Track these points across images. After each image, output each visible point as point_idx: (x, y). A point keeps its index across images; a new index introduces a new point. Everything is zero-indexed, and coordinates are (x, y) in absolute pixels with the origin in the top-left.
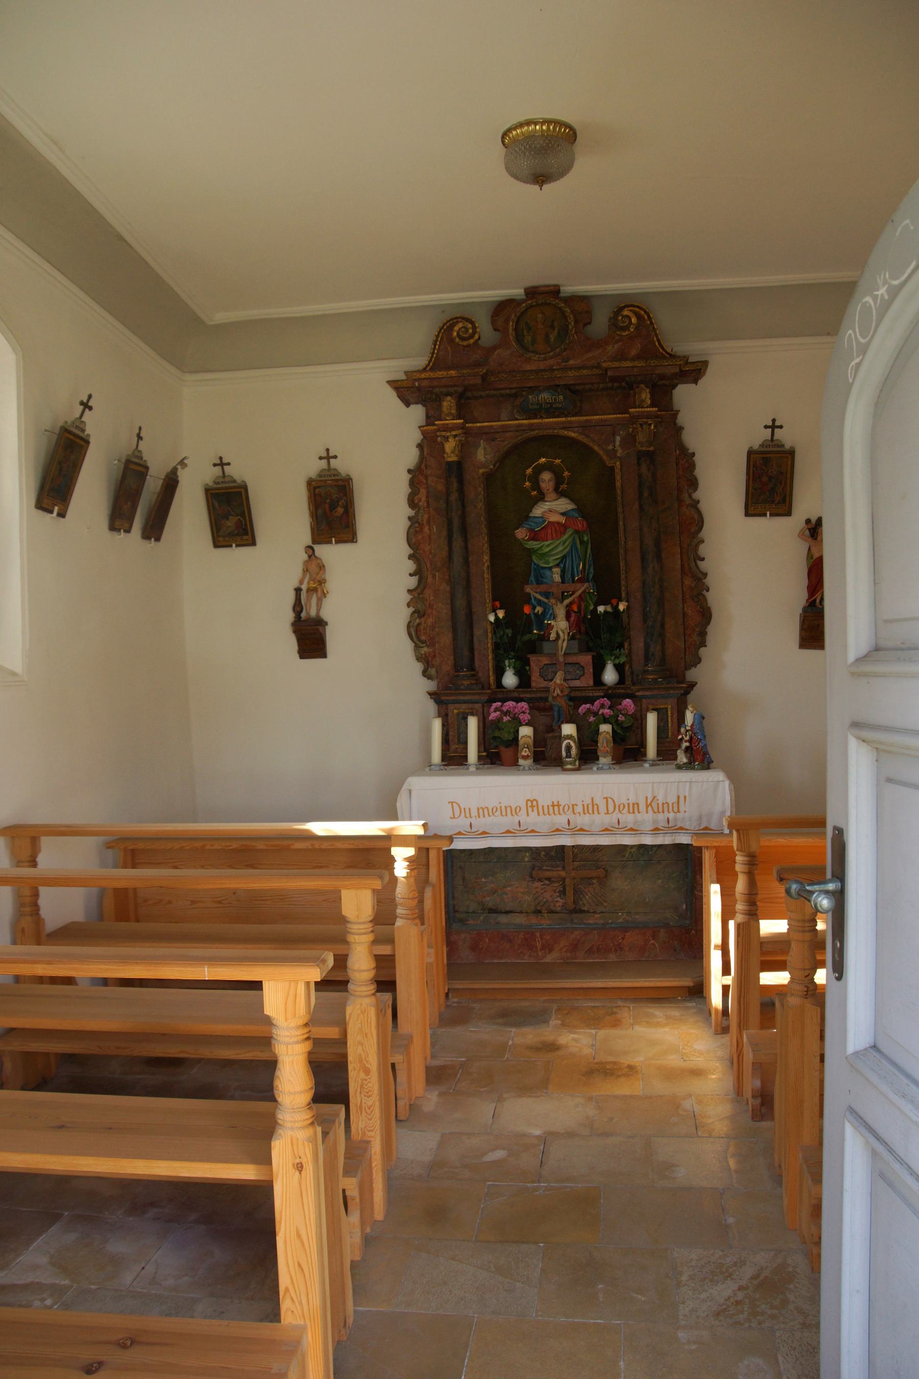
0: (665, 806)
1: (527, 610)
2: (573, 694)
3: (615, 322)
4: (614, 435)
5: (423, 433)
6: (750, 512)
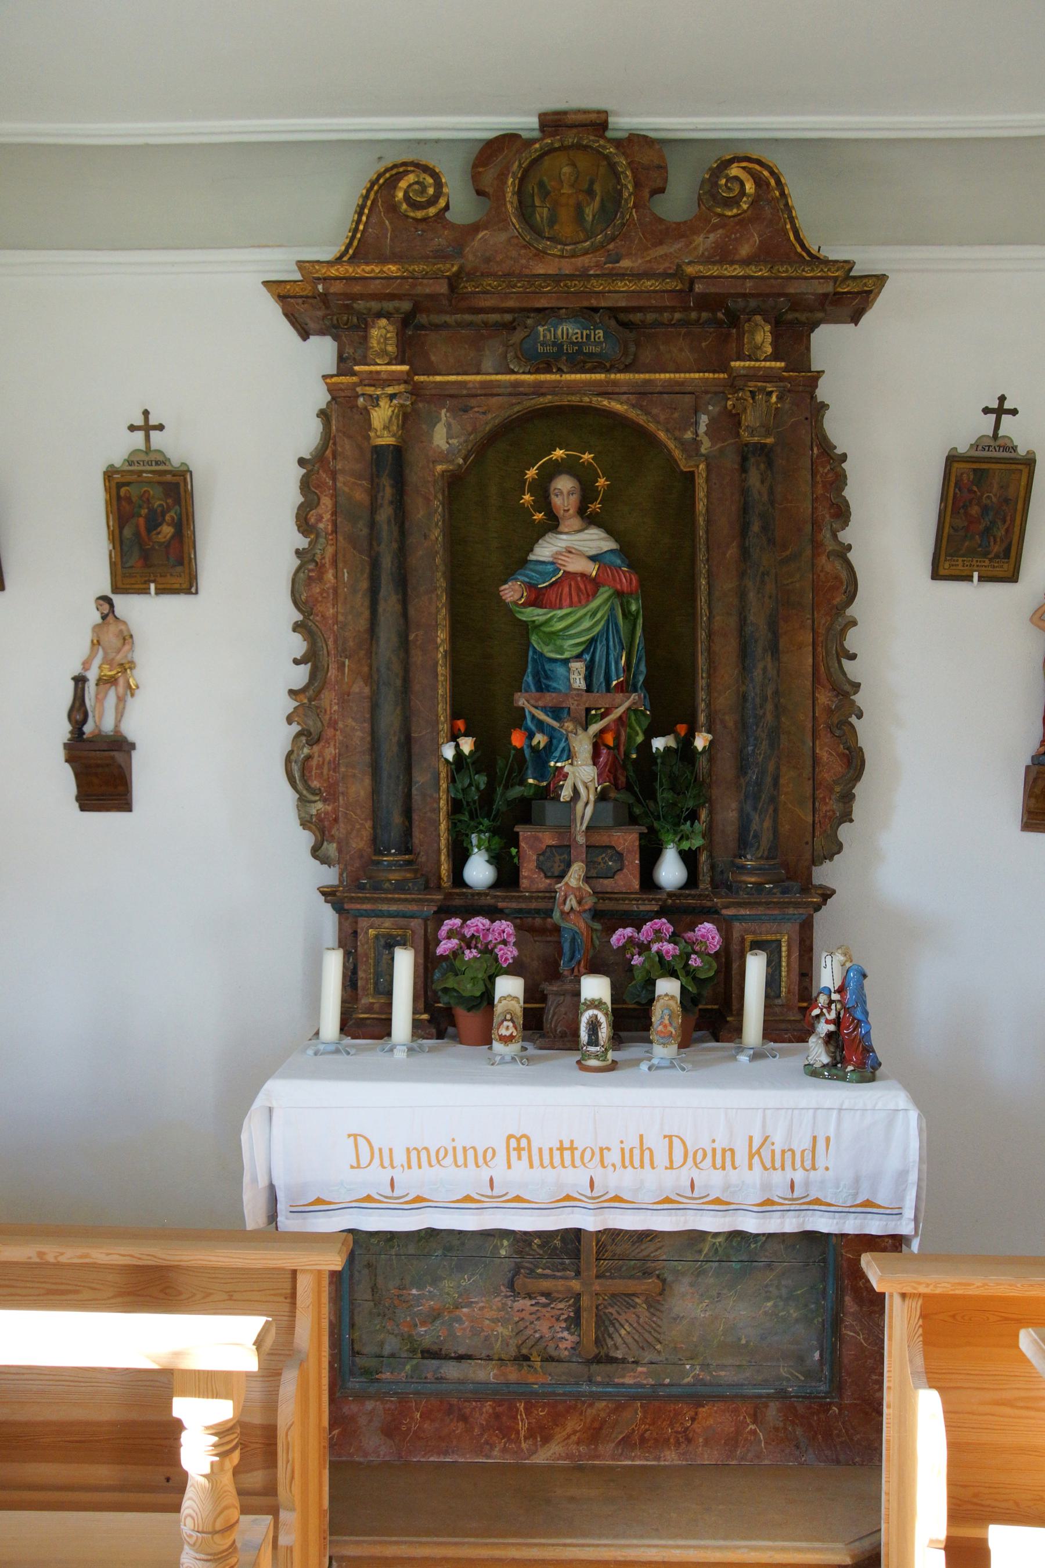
0: (788, 1155)
1: (517, 739)
2: (601, 906)
3: (713, 189)
5: (331, 389)
6: (942, 572)
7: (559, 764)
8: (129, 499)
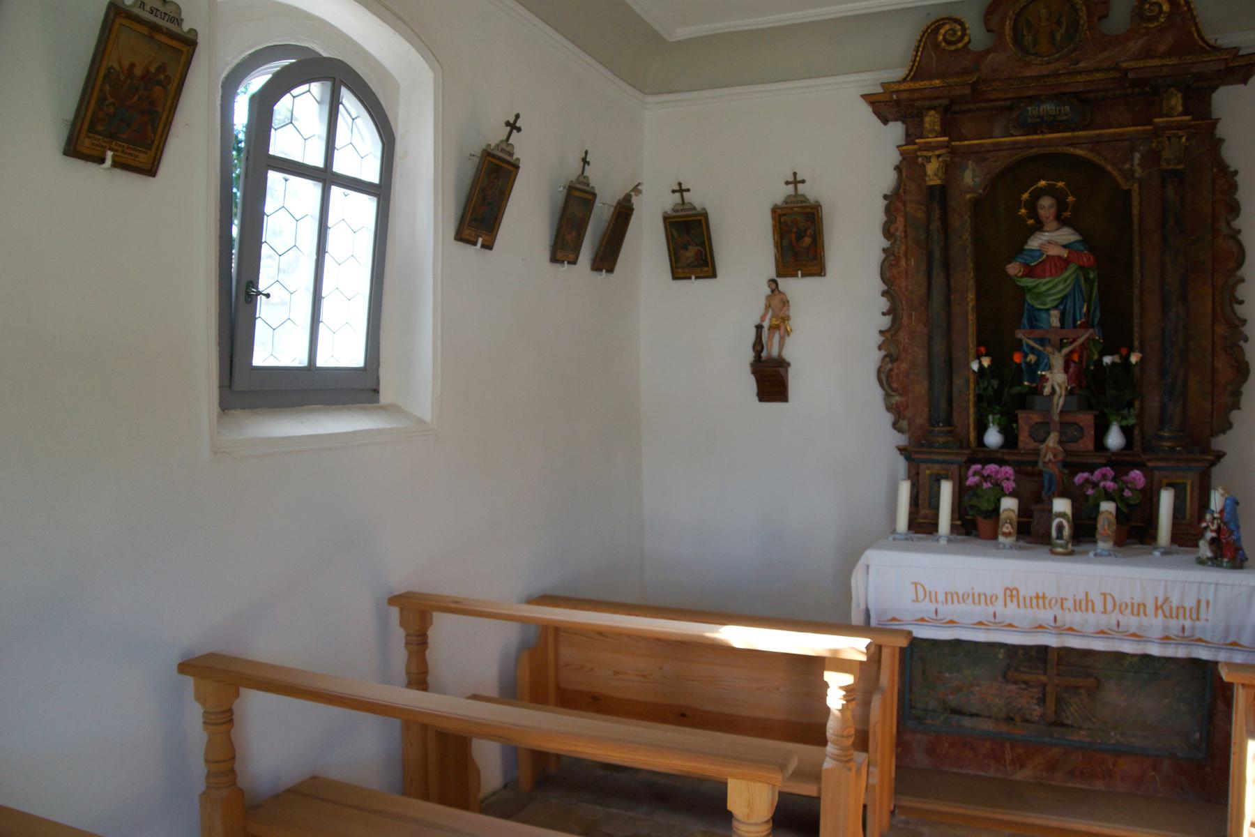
0: (1181, 611)
1: (1017, 358)
2: (1069, 459)
4: (1132, 150)
5: (902, 154)
8: (786, 224)
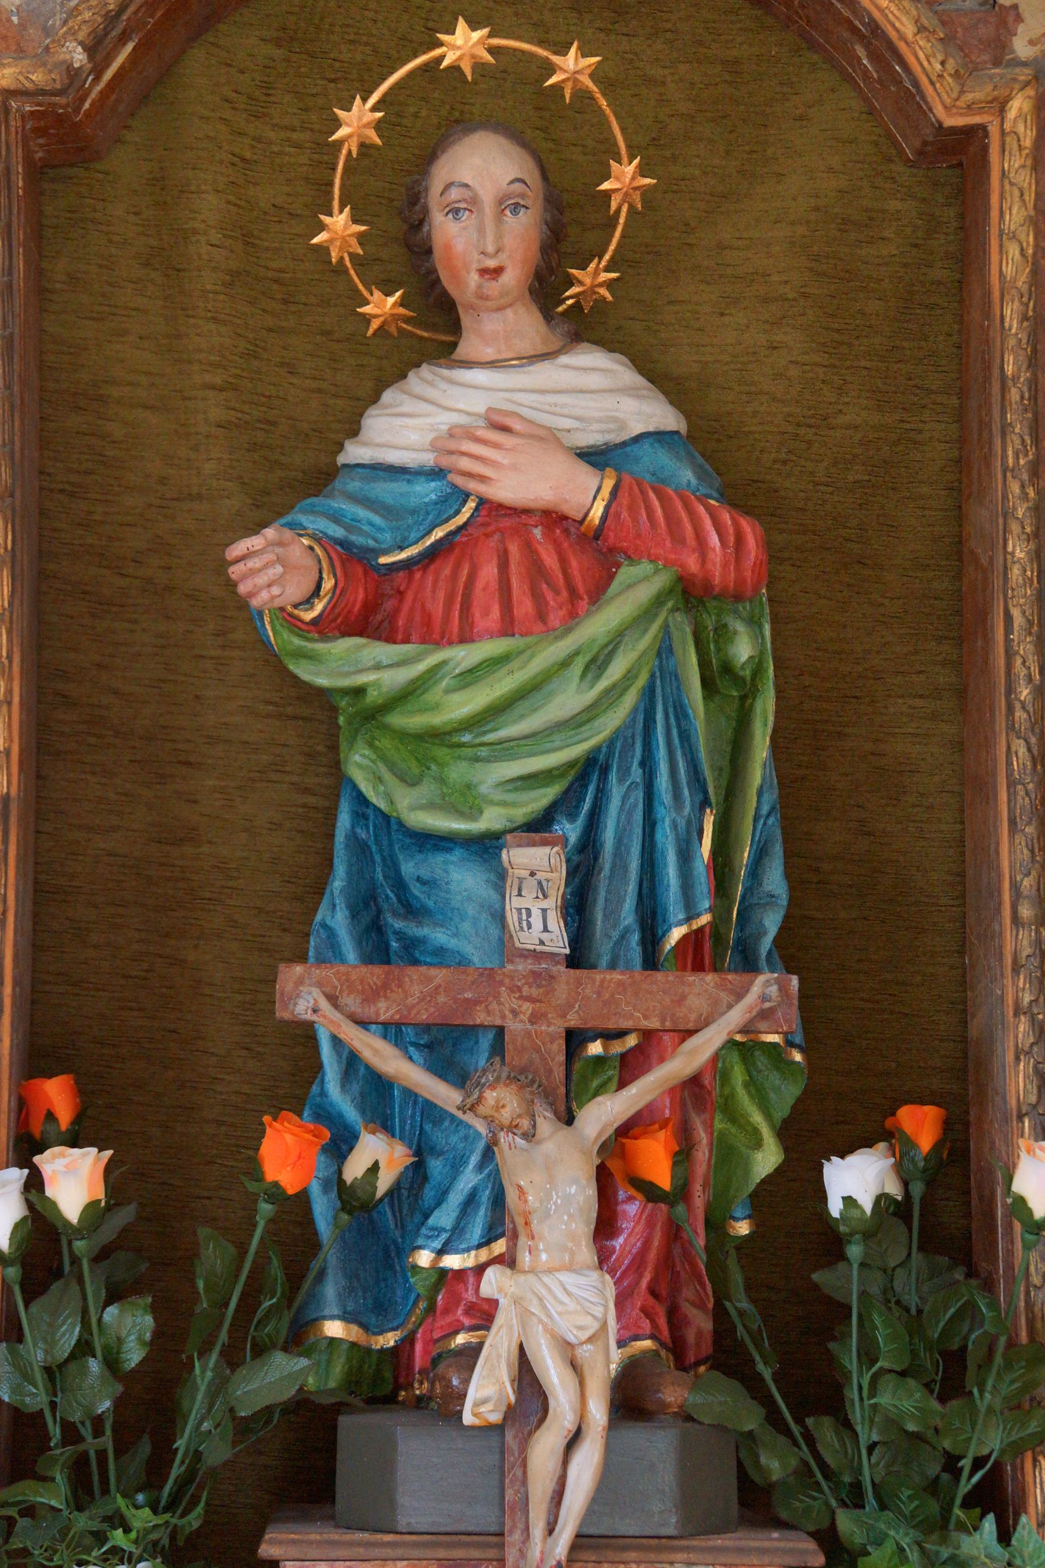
1: (285, 1156)
7: (452, 1261)
